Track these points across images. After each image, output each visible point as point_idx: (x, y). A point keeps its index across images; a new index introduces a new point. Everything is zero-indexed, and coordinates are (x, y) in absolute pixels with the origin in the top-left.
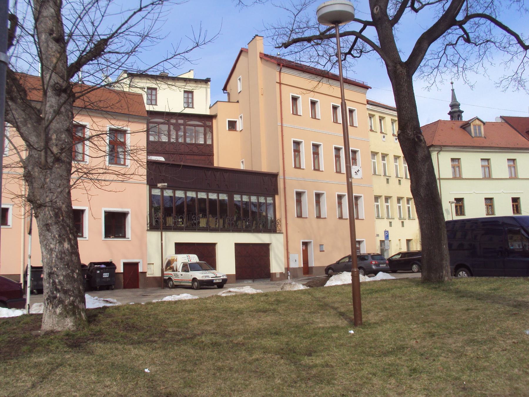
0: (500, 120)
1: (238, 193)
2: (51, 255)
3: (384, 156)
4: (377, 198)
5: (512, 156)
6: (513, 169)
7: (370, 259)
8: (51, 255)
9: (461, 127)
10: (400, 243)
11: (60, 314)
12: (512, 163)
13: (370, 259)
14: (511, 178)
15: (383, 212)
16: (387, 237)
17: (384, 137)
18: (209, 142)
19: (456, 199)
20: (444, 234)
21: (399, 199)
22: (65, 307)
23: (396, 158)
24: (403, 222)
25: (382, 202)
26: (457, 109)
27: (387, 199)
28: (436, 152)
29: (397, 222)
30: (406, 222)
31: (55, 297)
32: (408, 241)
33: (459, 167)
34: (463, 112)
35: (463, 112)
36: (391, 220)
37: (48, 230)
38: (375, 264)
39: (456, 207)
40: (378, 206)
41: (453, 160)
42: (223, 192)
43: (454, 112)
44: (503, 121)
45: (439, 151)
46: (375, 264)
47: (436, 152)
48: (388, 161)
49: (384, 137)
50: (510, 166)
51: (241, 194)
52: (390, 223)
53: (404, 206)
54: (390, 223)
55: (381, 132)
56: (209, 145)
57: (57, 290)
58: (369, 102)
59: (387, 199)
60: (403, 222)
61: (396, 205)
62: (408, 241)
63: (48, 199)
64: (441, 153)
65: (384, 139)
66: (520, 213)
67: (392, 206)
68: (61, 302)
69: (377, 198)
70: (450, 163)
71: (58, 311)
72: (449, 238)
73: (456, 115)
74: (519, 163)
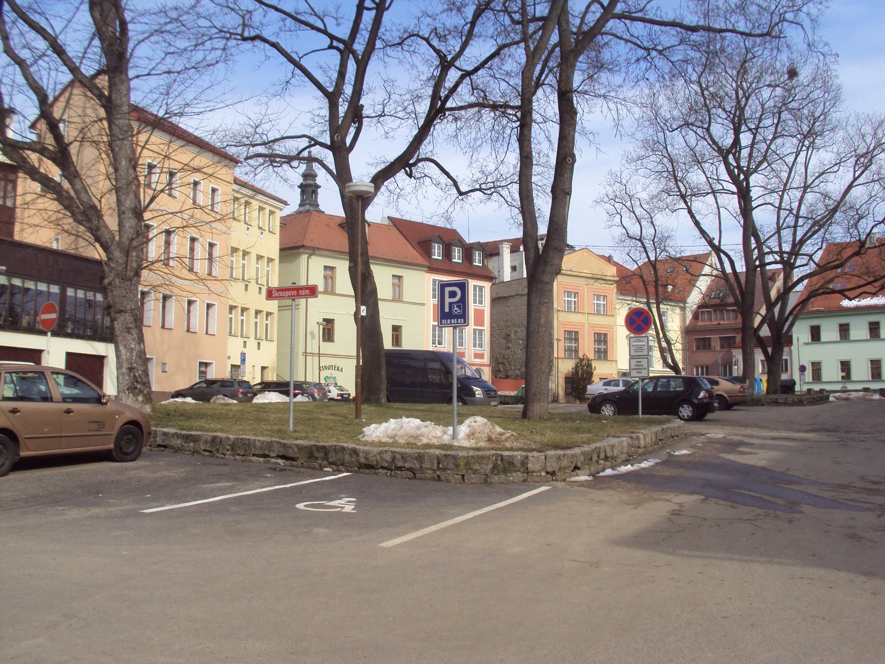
0: (387, 222)
1: (71, 285)
2: (131, 353)
3: (245, 253)
4: (232, 308)
5: (398, 271)
6: (397, 289)
7: (236, 385)
8: (131, 353)
9: (340, 225)
10: (254, 370)
11: (143, 401)
12: (397, 281)
13: (236, 385)
14: (394, 300)
15: (236, 328)
16: (243, 360)
17: (248, 229)
18: (9, 203)
19: (324, 320)
20: (383, 361)
21: (257, 312)
22: (145, 396)
23: (270, 260)
24: (259, 344)
25: (236, 315)
26: (311, 182)
27: (244, 310)
28: (306, 256)
29: (252, 343)
30: (264, 343)
31: (136, 388)
32: (263, 368)
33: (332, 278)
34: (320, 187)
35: (320, 187)
36: (245, 340)
37: (129, 333)
38: (242, 393)
39: (324, 329)
40: (231, 319)
41: (326, 268)
42: (55, 283)
43: (309, 185)
44: (391, 224)
45: (310, 255)
46: (242, 393)
47: (306, 256)
48: (249, 261)
49: (248, 229)
50: (394, 285)
51: (76, 287)
52: (245, 342)
53: (236, 318)
54: (245, 342)
55: (246, 223)
56: (9, 208)
57: (137, 382)
58: (236, 181)
59: (244, 310)
60: (259, 344)
61: (253, 320)
62: (263, 368)
63: (128, 307)
64: (313, 257)
65: (247, 232)
66: (400, 346)
67: (272, 325)
68: (141, 392)
69: (232, 308)
70: (322, 272)
71: (140, 398)
72: (387, 366)
73: (310, 190)
74: (405, 281)
